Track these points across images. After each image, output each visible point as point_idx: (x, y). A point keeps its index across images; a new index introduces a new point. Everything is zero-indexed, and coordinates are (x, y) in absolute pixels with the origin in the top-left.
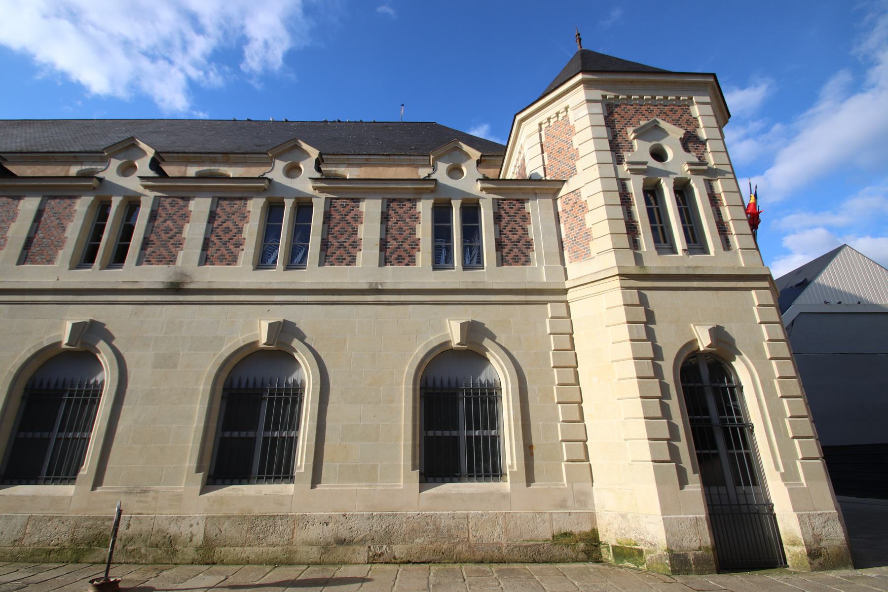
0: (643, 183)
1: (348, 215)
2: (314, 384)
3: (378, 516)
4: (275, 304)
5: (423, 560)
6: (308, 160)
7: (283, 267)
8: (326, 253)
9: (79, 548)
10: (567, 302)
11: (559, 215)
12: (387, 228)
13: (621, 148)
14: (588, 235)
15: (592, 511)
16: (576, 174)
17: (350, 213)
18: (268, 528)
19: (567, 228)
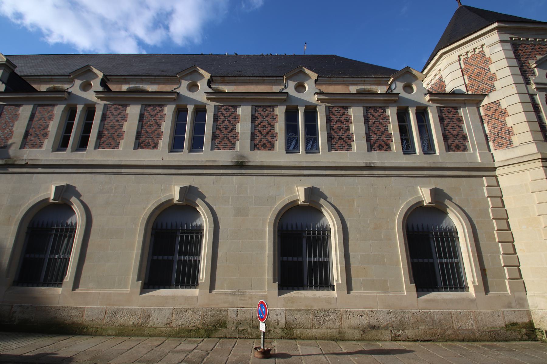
0: (546, 97)
1: (341, 118)
2: (338, 228)
3: (394, 312)
4: (308, 176)
5: (427, 339)
6: (203, 80)
7: (187, 151)
8: (331, 143)
9: (208, 328)
10: (496, 176)
11: (482, 118)
12: (368, 126)
13: (527, 74)
14: (510, 132)
15: (528, 310)
16: (495, 90)
17: (343, 116)
18: (325, 317)
19: (490, 127)
